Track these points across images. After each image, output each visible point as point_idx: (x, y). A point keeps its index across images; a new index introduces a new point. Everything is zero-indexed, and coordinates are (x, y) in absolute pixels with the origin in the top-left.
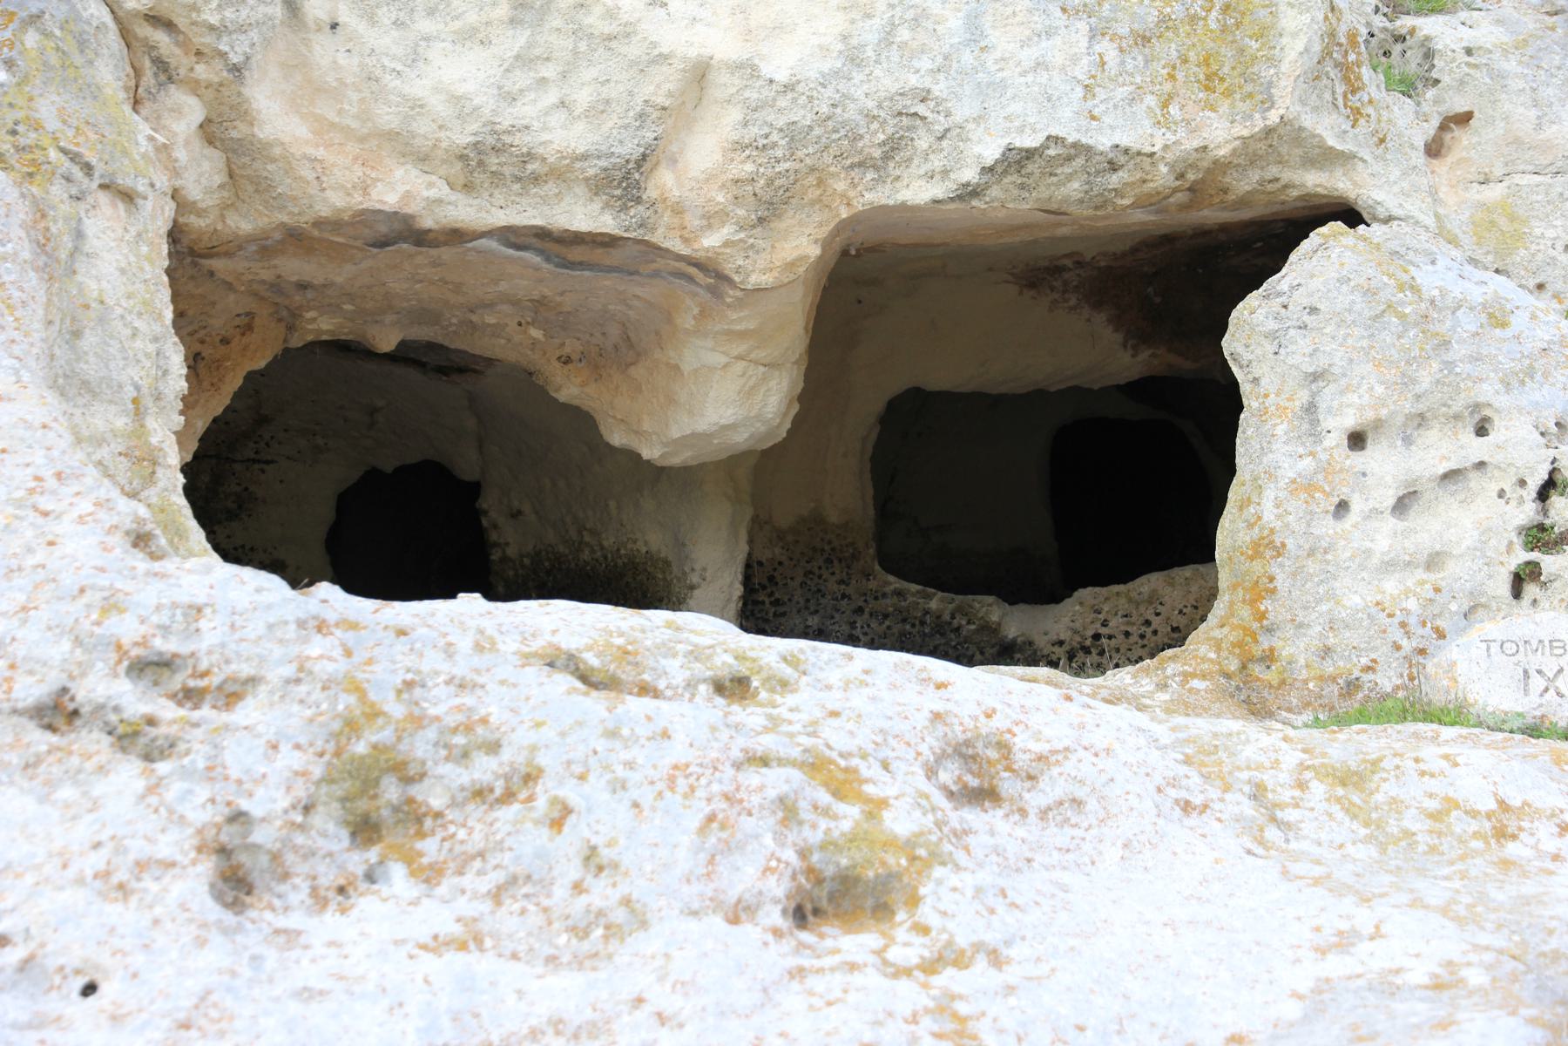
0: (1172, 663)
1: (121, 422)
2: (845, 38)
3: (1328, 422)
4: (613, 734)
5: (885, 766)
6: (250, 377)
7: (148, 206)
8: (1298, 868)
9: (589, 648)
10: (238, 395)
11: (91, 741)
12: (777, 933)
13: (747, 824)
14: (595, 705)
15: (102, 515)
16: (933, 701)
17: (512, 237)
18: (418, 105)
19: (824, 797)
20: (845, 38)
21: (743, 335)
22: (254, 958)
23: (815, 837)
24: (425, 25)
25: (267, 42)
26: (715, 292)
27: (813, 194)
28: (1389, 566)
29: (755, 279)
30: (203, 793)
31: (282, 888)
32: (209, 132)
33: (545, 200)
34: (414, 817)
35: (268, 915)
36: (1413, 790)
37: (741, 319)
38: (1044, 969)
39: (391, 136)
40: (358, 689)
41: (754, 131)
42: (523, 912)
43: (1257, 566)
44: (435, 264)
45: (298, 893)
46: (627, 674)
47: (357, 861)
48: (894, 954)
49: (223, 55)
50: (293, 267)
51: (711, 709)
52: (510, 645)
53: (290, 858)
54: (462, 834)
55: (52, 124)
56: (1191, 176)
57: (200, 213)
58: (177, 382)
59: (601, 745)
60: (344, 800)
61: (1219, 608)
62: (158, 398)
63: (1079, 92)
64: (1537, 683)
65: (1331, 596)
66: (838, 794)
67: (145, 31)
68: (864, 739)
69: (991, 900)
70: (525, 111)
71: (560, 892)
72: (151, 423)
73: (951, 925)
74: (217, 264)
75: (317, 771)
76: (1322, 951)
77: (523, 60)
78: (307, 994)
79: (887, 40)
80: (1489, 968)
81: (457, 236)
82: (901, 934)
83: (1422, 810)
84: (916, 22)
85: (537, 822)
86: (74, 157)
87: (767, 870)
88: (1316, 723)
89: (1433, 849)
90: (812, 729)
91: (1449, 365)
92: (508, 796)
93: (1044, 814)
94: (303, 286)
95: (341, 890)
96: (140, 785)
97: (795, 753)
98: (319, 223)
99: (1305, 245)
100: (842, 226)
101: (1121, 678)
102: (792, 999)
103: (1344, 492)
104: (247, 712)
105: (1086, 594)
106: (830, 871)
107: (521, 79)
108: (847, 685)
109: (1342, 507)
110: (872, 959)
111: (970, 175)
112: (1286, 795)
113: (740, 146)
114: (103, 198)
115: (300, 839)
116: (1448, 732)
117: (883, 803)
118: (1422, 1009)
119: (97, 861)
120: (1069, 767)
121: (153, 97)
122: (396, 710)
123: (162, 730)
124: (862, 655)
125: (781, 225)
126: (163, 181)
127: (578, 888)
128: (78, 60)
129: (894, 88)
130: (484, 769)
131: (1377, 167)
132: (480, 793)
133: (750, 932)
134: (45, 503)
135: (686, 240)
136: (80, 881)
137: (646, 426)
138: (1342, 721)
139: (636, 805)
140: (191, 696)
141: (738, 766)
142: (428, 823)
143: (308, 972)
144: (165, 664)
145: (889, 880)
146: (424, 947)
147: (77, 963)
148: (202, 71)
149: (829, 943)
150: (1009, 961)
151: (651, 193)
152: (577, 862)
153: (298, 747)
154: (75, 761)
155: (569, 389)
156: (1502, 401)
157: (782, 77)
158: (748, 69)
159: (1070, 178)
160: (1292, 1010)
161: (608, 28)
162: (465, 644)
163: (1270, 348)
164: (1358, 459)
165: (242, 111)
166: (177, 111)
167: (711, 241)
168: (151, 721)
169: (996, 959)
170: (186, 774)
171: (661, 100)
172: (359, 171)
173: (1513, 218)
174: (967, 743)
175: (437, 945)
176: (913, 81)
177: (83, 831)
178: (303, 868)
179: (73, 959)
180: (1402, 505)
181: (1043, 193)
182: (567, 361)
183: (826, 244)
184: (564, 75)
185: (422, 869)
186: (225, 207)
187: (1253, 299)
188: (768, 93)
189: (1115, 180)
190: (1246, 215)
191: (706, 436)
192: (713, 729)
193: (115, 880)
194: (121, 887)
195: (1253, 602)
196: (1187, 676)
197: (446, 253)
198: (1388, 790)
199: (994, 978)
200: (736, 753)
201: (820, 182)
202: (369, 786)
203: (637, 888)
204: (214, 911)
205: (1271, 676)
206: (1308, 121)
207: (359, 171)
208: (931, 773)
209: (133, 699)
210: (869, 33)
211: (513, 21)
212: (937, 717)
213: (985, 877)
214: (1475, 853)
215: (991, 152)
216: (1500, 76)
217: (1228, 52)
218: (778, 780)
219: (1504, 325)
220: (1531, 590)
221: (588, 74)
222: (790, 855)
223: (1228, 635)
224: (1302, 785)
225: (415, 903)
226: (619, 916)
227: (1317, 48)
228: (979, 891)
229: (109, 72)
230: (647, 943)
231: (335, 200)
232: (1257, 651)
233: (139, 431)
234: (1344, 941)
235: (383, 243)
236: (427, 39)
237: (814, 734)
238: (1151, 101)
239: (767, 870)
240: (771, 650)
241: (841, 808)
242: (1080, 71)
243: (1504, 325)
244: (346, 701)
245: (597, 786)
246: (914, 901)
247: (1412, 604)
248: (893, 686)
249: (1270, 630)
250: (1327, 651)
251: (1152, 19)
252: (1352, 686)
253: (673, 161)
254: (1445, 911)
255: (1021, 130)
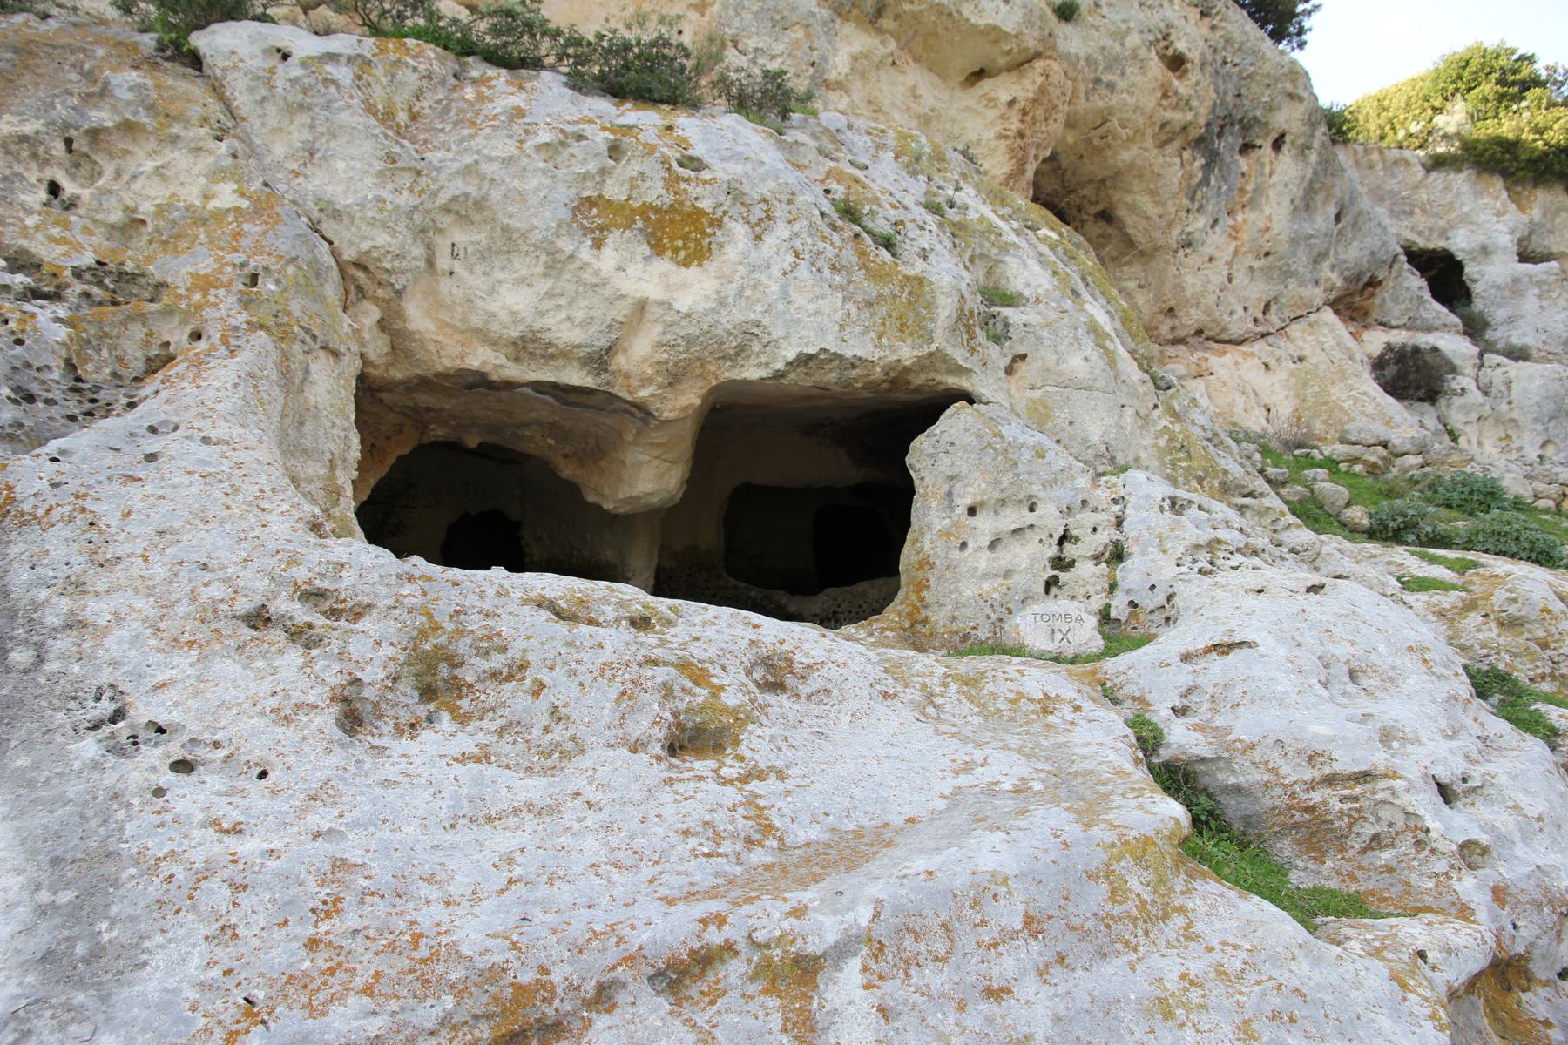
0: (876, 623)
1: (322, 472)
2: (718, 292)
3: (958, 501)
4: (571, 644)
5: (724, 668)
6: (400, 459)
7: (346, 359)
8: (943, 728)
9: (561, 598)
10: (393, 468)
11: (277, 635)
12: (658, 758)
13: (645, 697)
14: (561, 628)
15: (294, 512)
16: (751, 635)
17: (538, 386)
18: (493, 316)
19: (688, 684)
20: (718, 292)
21: (659, 445)
22: (358, 762)
23: (682, 706)
24: (499, 275)
25: (416, 280)
26: (645, 421)
27: (699, 371)
28: (986, 576)
29: (667, 415)
30: (336, 668)
31: (378, 723)
32: (382, 325)
33: (557, 368)
34: (457, 687)
35: (369, 738)
36: (1002, 688)
37: (657, 437)
38: (808, 781)
39: (478, 331)
40: (429, 615)
41: (668, 337)
42: (515, 742)
43: (920, 573)
44: (499, 400)
45: (387, 727)
46: (582, 613)
47: (422, 710)
48: (724, 771)
49: (392, 285)
50: (424, 399)
51: (626, 633)
52: (517, 594)
53: (384, 706)
54: (483, 697)
55: (297, 313)
56: (892, 374)
57: (375, 367)
58: (355, 453)
59: (563, 650)
60: (416, 675)
61: (901, 595)
62: (344, 461)
63: (837, 327)
64: (1058, 636)
65: (957, 590)
66: (697, 683)
67: (353, 271)
68: (712, 652)
69: (779, 743)
70: (550, 321)
71: (536, 732)
72: (339, 473)
73: (756, 756)
74: (384, 396)
75: (402, 659)
76: (957, 773)
77: (549, 295)
78: (386, 783)
79: (740, 294)
80: (1043, 781)
81: (509, 385)
82: (728, 761)
83: (1007, 699)
84: (755, 287)
85: (525, 692)
86: (307, 331)
87: (655, 723)
88: (949, 655)
89: (1011, 719)
90: (684, 648)
91: (1018, 475)
92: (510, 678)
93: (809, 697)
94: (428, 410)
95: (412, 726)
96: (301, 661)
97: (673, 659)
98: (437, 375)
99: (948, 412)
100: (713, 390)
101: (850, 629)
102: (665, 796)
103: (965, 537)
104: (364, 624)
105: (830, 591)
106: (690, 725)
107: (548, 304)
108: (704, 624)
109: (964, 545)
110: (711, 774)
111: (780, 366)
112: (937, 690)
113: (661, 344)
114: (322, 353)
115: (390, 696)
116: (1016, 660)
117: (721, 688)
118: (1010, 804)
119: (273, 702)
120: (824, 672)
121: (354, 305)
122: (450, 626)
123: (316, 631)
124: (713, 609)
125: (681, 387)
126: (355, 348)
127: (546, 730)
128: (315, 282)
129: (743, 319)
130: (497, 661)
131: (983, 377)
132: (494, 675)
133: (643, 758)
134: (264, 504)
135: (630, 393)
136: (263, 714)
137: (607, 491)
138: (962, 654)
139: (581, 684)
140: (334, 613)
141: (640, 665)
142: (464, 690)
143: (390, 772)
144: (321, 594)
145: (722, 731)
146: (456, 760)
147: (257, 760)
148: (380, 293)
149: (688, 765)
150: (788, 777)
151: (613, 367)
152: (546, 715)
153: (392, 644)
154: (266, 646)
155: (567, 471)
156: (1042, 494)
157: (684, 310)
158: (666, 305)
159: (831, 370)
160: (941, 804)
161: (595, 281)
162: (491, 592)
163: (930, 462)
164: (972, 521)
165: (400, 315)
166: (366, 313)
167: (643, 394)
168: (310, 626)
169: (781, 776)
170: (326, 655)
171: (620, 318)
172: (459, 349)
173: (1046, 407)
174: (769, 657)
175: (464, 759)
176: (752, 316)
177: (267, 686)
178: (391, 712)
179: (254, 758)
180: (993, 545)
181: (817, 377)
182: (566, 456)
183: (704, 399)
184: (570, 304)
185: (459, 716)
186: (388, 365)
187: (922, 437)
188: (677, 318)
189: (854, 373)
190: (918, 397)
191: (637, 498)
192: (628, 644)
193: (282, 714)
194: (286, 717)
195: (918, 592)
196: (883, 630)
197: (504, 395)
198: (989, 688)
199: (780, 786)
200: (640, 658)
201: (702, 366)
202: (432, 668)
203: (580, 731)
204: (338, 734)
205: (925, 630)
206: (950, 351)
207: (459, 349)
208: (748, 673)
209: (301, 613)
210: (731, 290)
211: (545, 275)
212: (753, 642)
213: (776, 730)
214: (1033, 721)
215: (791, 355)
216: (1039, 338)
217: (911, 314)
218: (662, 674)
219: (1043, 457)
220: (1054, 590)
221: (583, 304)
222: (667, 715)
223: (905, 609)
224: (945, 685)
225: (453, 735)
226: (569, 746)
227: (955, 315)
228: (772, 737)
229: (331, 290)
230: (586, 762)
231: (446, 363)
232: (919, 618)
233: (332, 477)
234: (968, 767)
235: (470, 387)
236: (500, 282)
237: (684, 650)
238: (873, 335)
239: (655, 723)
240: (663, 604)
241: (698, 690)
242: (838, 317)
243: (1043, 457)
244: (421, 620)
245: (560, 672)
246: (737, 742)
247: (996, 596)
248: (729, 626)
249: (926, 607)
250: (954, 619)
251: (874, 294)
252: (966, 637)
253: (625, 351)
254: (1019, 751)
255: (807, 345)
